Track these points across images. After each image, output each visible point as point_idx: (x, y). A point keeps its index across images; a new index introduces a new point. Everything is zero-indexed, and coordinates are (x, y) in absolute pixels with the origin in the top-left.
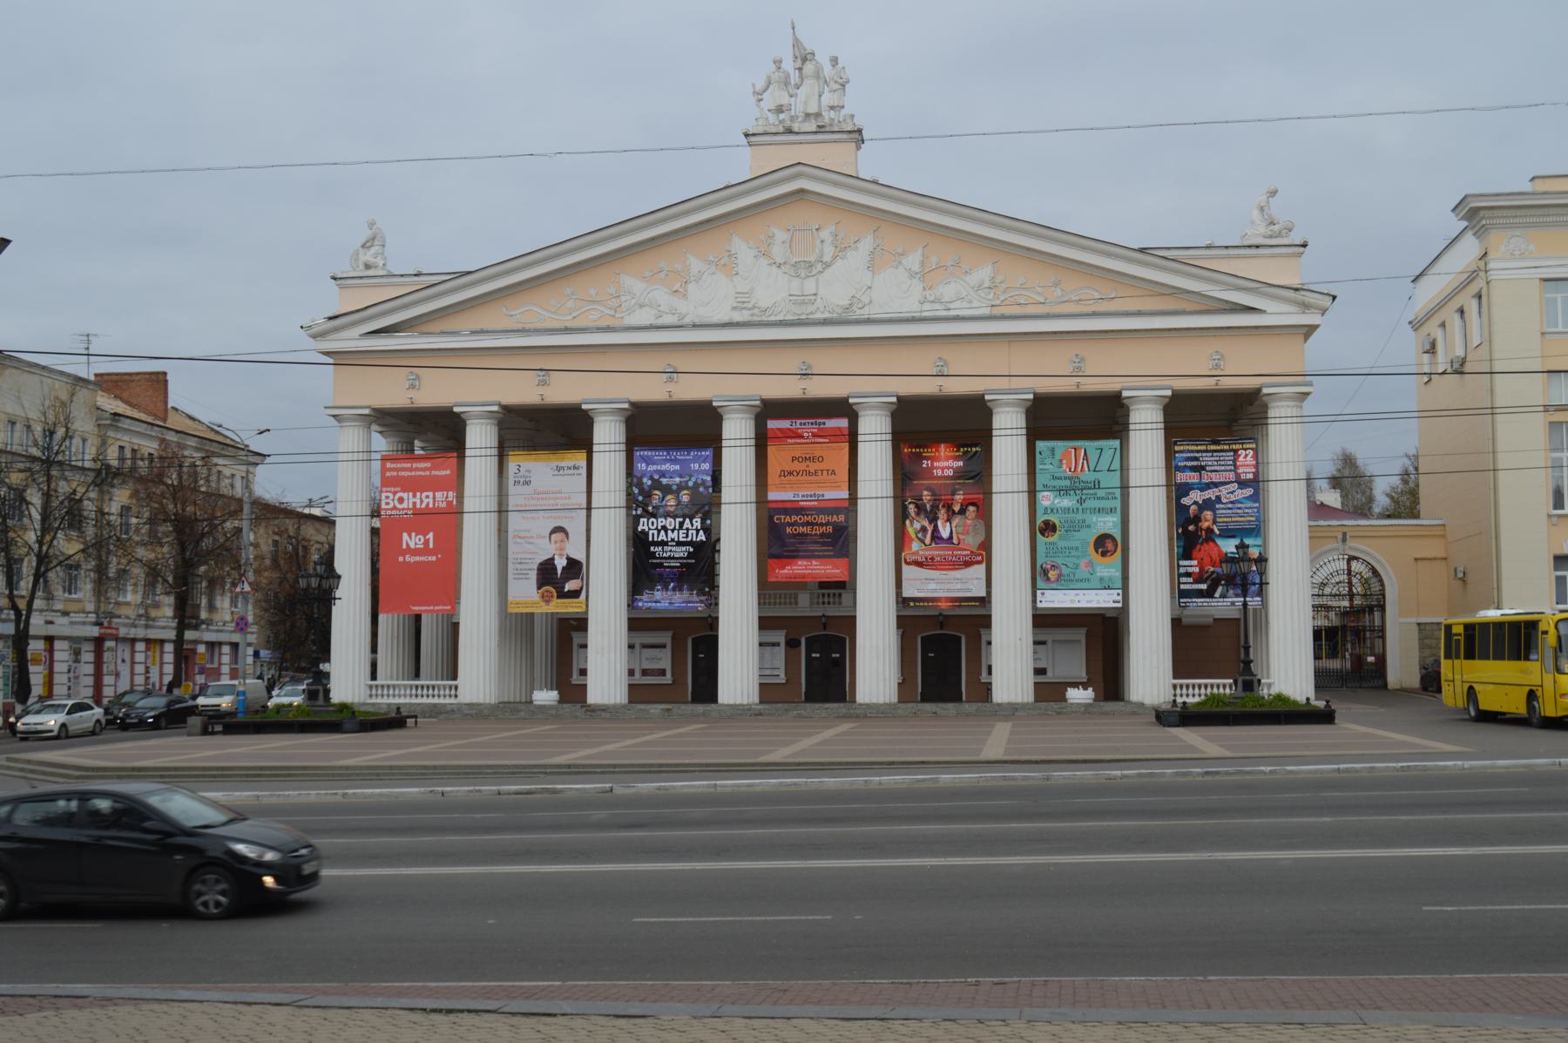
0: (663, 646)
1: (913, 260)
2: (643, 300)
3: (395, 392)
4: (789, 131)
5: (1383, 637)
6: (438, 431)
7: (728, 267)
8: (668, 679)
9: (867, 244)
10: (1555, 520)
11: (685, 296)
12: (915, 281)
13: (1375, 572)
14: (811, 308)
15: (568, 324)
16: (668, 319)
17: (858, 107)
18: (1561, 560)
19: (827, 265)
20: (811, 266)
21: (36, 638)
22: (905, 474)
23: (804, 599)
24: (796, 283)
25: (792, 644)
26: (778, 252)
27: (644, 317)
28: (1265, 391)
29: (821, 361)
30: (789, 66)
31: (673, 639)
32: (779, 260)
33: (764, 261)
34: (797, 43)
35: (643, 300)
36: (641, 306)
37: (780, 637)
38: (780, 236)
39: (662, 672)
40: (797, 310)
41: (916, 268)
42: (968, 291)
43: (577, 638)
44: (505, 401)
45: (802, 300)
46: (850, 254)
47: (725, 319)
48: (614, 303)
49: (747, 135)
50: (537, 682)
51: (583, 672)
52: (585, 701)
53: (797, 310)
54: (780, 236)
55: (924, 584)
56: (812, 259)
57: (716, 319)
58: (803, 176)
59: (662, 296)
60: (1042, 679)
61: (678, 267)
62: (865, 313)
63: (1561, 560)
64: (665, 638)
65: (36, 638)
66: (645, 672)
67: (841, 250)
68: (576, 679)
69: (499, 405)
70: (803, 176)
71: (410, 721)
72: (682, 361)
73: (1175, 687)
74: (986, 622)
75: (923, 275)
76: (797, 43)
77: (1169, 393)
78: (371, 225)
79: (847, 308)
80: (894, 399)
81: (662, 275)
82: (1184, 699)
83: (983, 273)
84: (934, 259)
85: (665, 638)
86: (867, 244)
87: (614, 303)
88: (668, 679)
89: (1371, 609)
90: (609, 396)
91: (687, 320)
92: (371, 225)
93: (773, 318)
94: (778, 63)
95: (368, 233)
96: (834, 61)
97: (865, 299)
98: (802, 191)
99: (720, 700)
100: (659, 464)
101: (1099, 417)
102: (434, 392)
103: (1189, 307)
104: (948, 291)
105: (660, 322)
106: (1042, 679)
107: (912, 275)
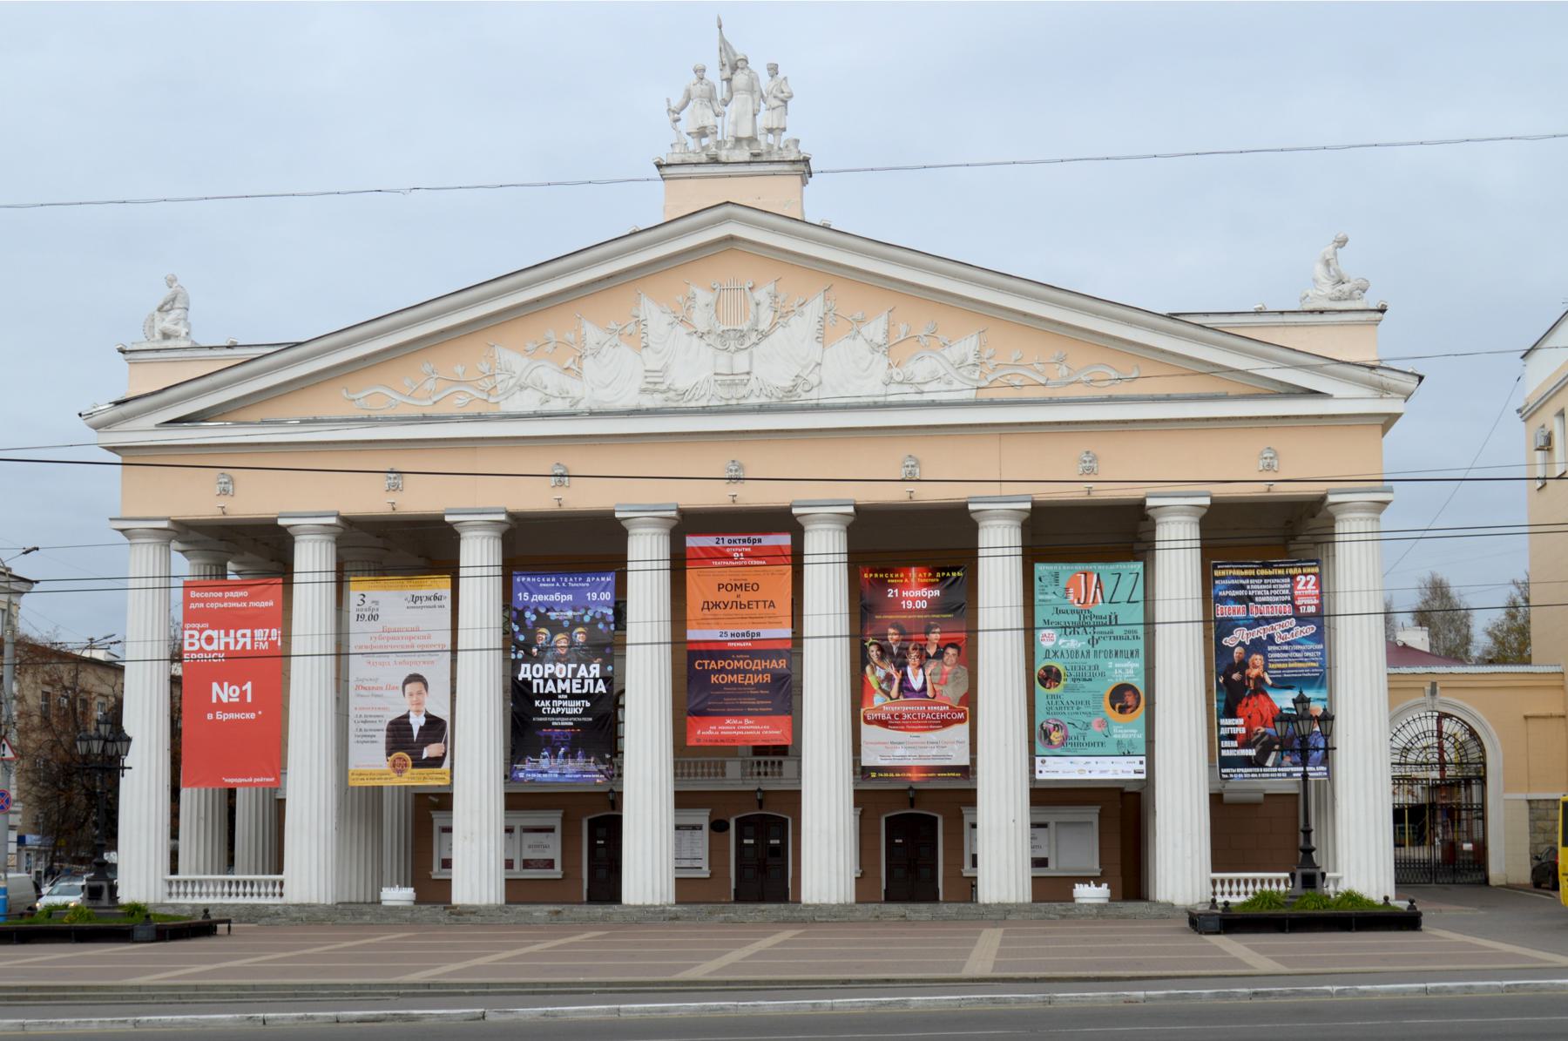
0: (551, 830)
1: (876, 329)
2: (524, 380)
3: (202, 499)
4: (715, 161)
5: (1484, 819)
6: (262, 549)
7: (636, 337)
8: (557, 872)
9: (815, 307)
11: (579, 375)
12: (878, 356)
13: (1473, 734)
14: (743, 391)
15: (428, 412)
16: (557, 405)
17: (804, 128)
19: (764, 335)
20: (742, 335)
22: (865, 607)
24: (723, 359)
25: (718, 826)
26: (700, 319)
27: (526, 402)
29: (758, 460)
30: (714, 75)
31: (564, 820)
32: (702, 328)
33: (681, 330)
34: (724, 46)
35: (524, 380)
36: (522, 388)
37: (702, 817)
38: (703, 297)
39: (550, 864)
41: (880, 339)
42: (946, 369)
43: (438, 819)
45: (732, 380)
46: (794, 320)
48: (488, 383)
49: (659, 166)
51: (447, 864)
53: (722, 392)
54: (703, 297)
56: (745, 326)
57: (619, 405)
58: (732, 217)
59: (549, 375)
60: (1042, 872)
61: (570, 336)
62: (813, 397)
64: (554, 819)
66: (527, 864)
67: (782, 315)
68: (437, 872)
69: (167, 519)
70: (732, 217)
71: (222, 928)
72: (576, 461)
73: (1214, 882)
74: (969, 798)
76: (724, 46)
77: (1207, 501)
79: (790, 391)
81: (549, 348)
82: (1227, 898)
83: (967, 346)
84: (903, 328)
85: (554, 819)
86: (815, 307)
87: (488, 383)
88: (557, 872)
89: (1468, 782)
90: (481, 505)
91: (581, 407)
92: (171, 281)
93: (693, 404)
94: (700, 72)
95: (167, 293)
96: (773, 70)
97: (814, 379)
98: (731, 239)
99: (981, 900)
101: (1119, 532)
102: (253, 499)
103: (1232, 390)
104: (920, 369)
105: (546, 408)
106: (1042, 872)
107: (874, 348)
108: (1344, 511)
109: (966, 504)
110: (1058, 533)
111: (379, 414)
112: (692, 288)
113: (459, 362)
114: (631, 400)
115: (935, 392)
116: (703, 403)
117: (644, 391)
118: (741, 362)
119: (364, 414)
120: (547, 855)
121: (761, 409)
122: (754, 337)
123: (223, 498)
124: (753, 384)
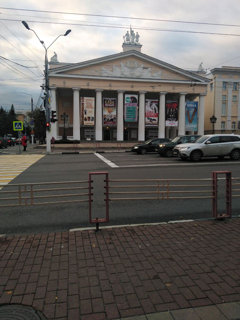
2: (106, 72)
7: (120, 66)
10: (233, 117)
14: (133, 76)
17: (140, 42)
22: (104, 102)
27: (106, 75)
28: (96, 90)
29: (113, 84)
35: (106, 72)
36: (105, 73)
38: (128, 63)
44: (168, 92)
47: (120, 76)
50: (157, 139)
52: (138, 140)
55: (174, 124)
58: (132, 52)
59: (109, 72)
62: (142, 77)
70: (132, 52)
72: (134, 84)
78: (55, 53)
92: (55, 53)
94: (128, 32)
96: (137, 33)
99: (117, 140)
104: (155, 75)
108: (201, 96)
109: (72, 88)
110: (85, 93)
112: (127, 62)
113: (97, 68)
115: (156, 78)
116: (128, 77)
117: (121, 75)
122: (135, 69)
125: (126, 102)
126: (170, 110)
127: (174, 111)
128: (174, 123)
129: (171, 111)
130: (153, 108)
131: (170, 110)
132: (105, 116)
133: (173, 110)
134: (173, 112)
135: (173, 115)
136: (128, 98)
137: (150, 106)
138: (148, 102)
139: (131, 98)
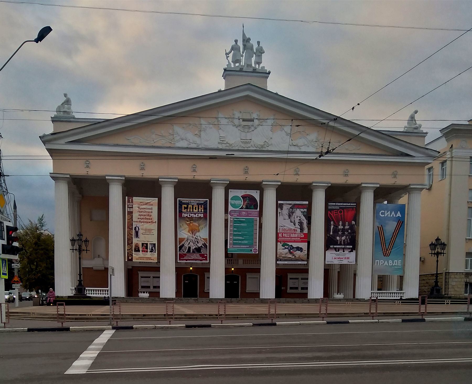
2: (183, 137)
3: (77, 168)
7: (217, 126)
11: (200, 136)
14: (249, 145)
18: (469, 254)
21: (420, 310)
22: (179, 209)
23: (241, 261)
24: (243, 134)
27: (183, 144)
28: (212, 182)
29: (353, 170)
34: (244, 35)
36: (182, 139)
40: (243, 145)
41: (289, 132)
44: (179, 177)
45: (245, 142)
47: (216, 147)
53: (243, 145)
57: (212, 146)
59: (190, 136)
62: (269, 149)
63: (469, 254)
65: (420, 310)
69: (124, 176)
70: (246, 91)
75: (290, 135)
76: (244, 35)
79: (262, 146)
80: (280, 183)
90: (373, 182)
91: (200, 147)
92: (65, 95)
93: (234, 148)
94: (236, 41)
95: (65, 99)
96: (259, 43)
97: (270, 143)
100: (388, 213)
103: (387, 154)
104: (300, 142)
111: (138, 144)
113: (163, 130)
114: (215, 146)
116: (237, 148)
117: (219, 143)
118: (249, 136)
119: (133, 144)
120: (143, 279)
121: (256, 151)
122: (253, 128)
123: (142, 171)
124: (252, 143)
125: (230, 208)
126: (336, 226)
127: (347, 227)
128: (347, 256)
129: (341, 227)
130: (297, 221)
131: (336, 226)
132: (181, 240)
133: (344, 225)
134: (343, 230)
135: (343, 238)
136: (235, 198)
137: (290, 216)
138: (285, 207)
139: (244, 197)
